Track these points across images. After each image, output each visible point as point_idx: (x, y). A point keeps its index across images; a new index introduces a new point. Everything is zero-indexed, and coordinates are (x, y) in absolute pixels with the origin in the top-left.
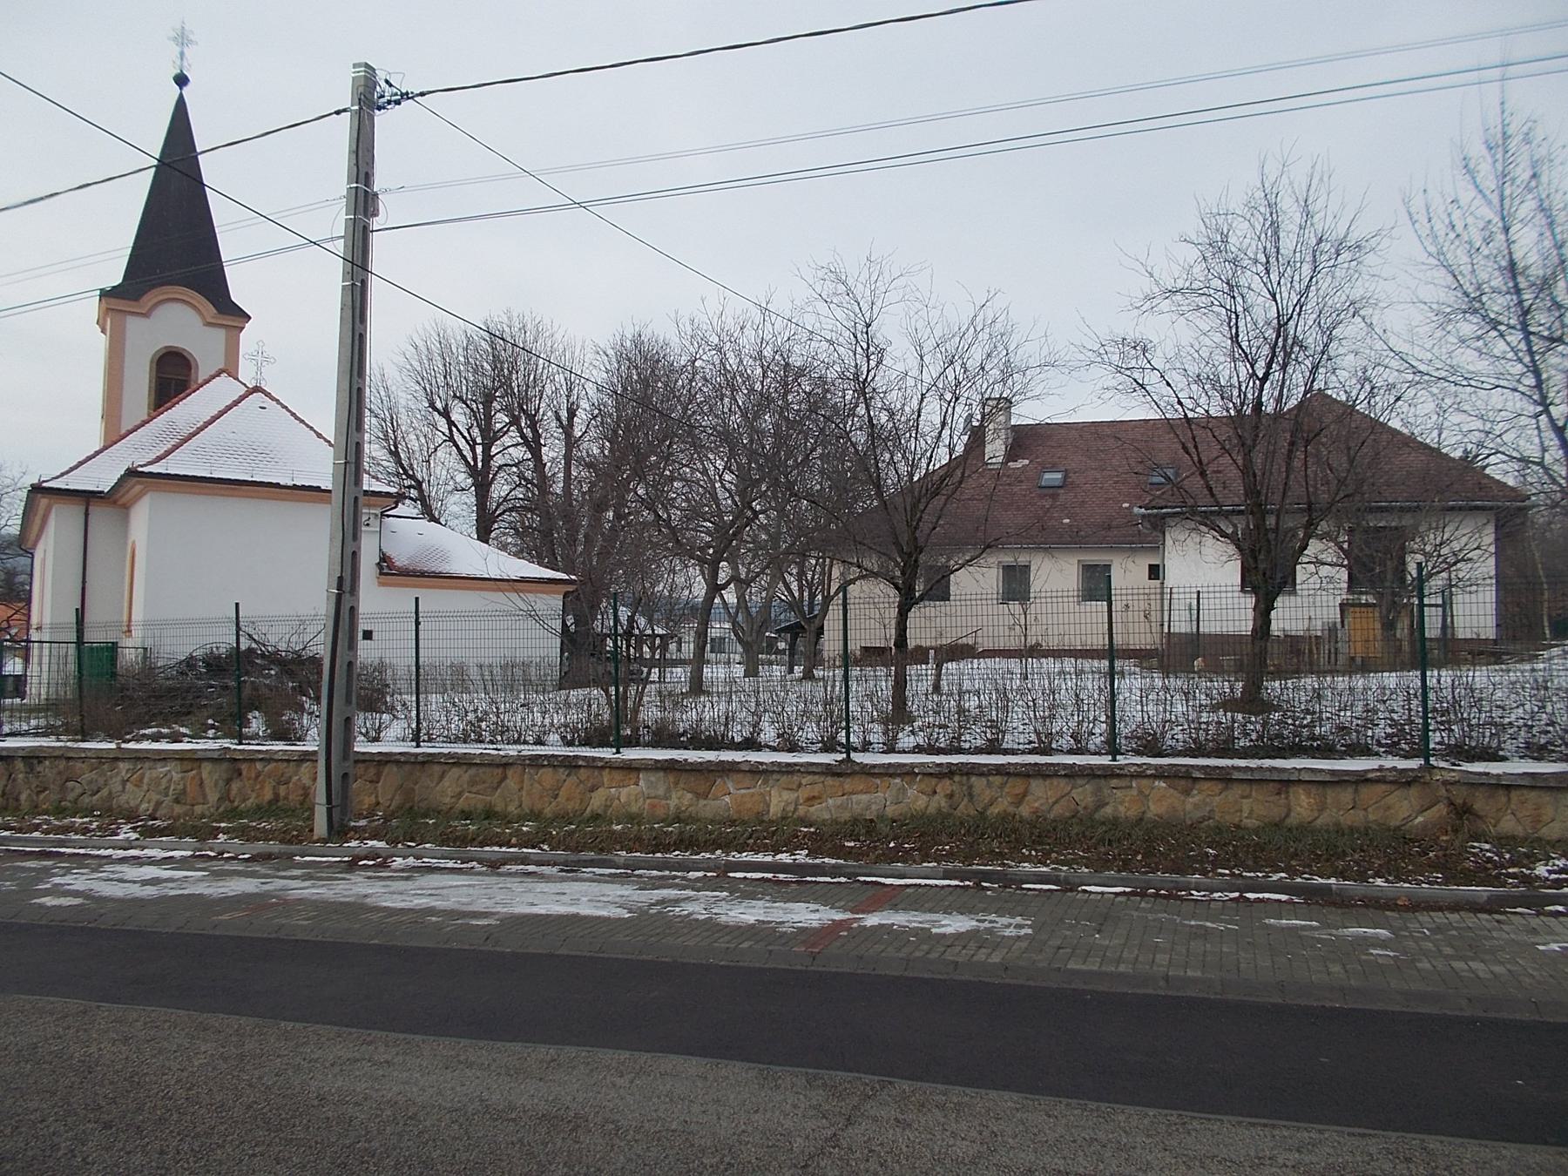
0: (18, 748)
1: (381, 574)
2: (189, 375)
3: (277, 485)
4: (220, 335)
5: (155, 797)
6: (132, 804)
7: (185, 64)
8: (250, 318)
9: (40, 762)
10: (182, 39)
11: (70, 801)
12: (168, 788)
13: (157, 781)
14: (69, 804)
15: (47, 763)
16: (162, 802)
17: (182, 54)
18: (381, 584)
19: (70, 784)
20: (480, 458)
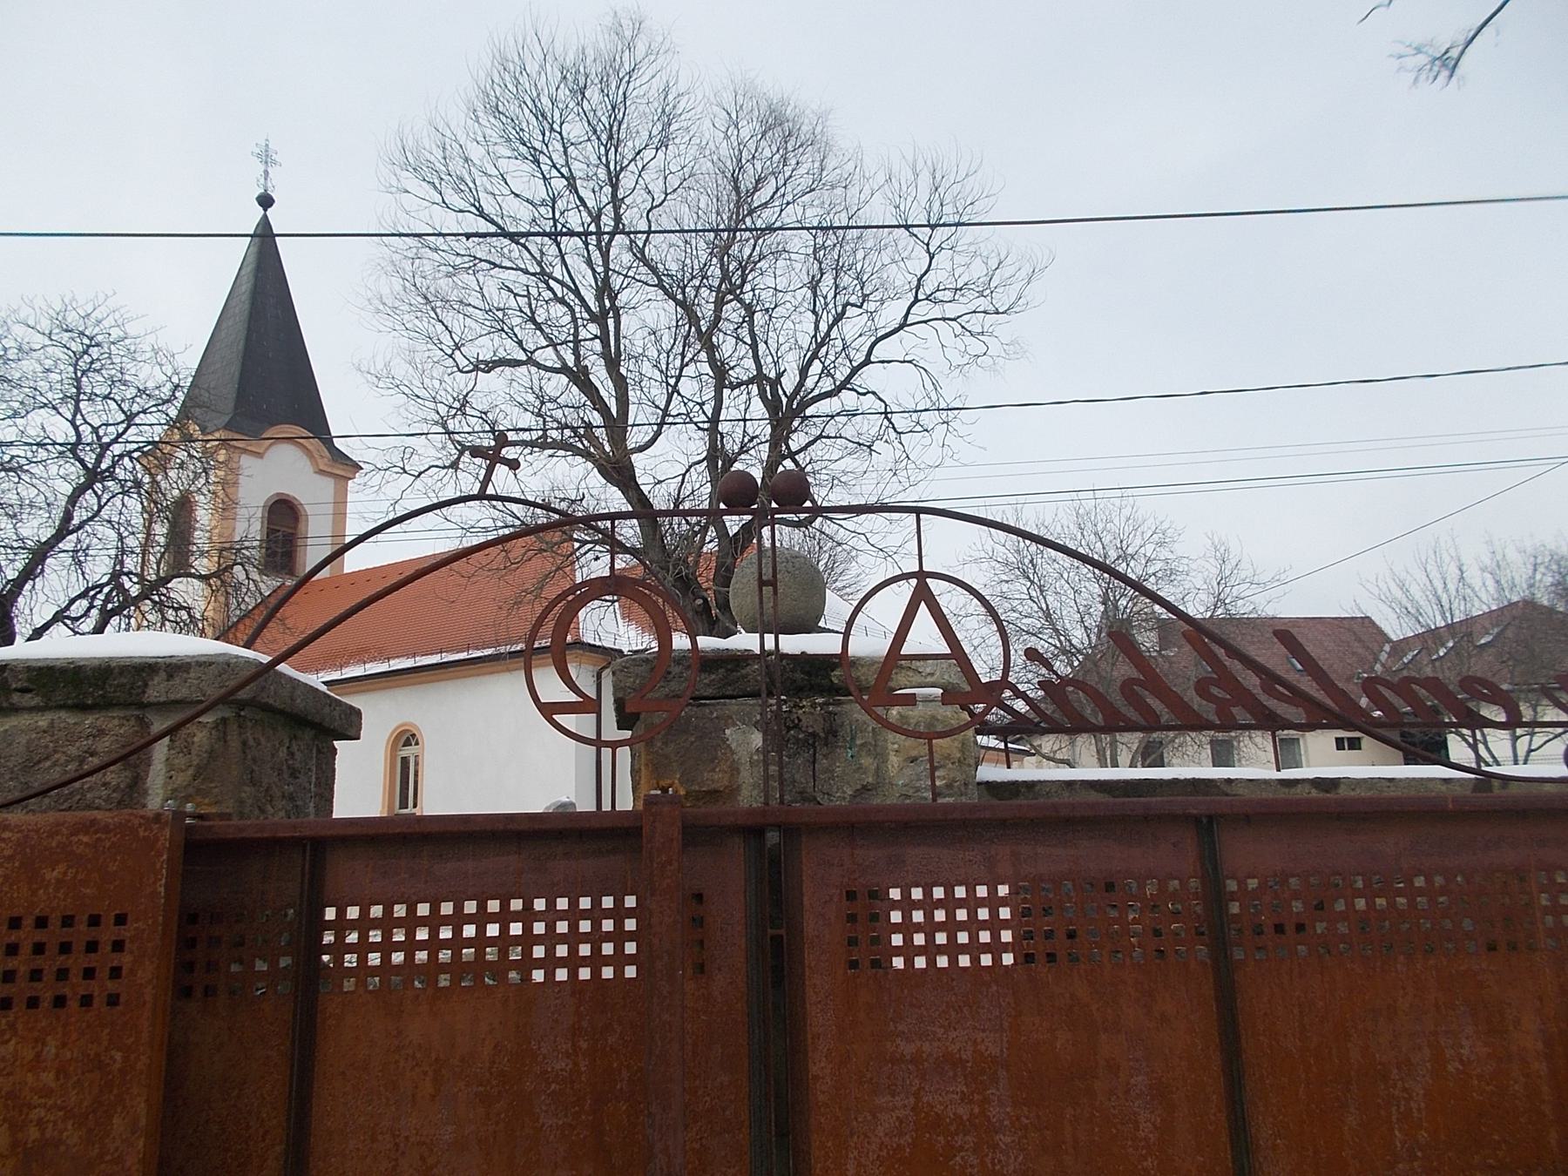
2: (295, 528)
7: (269, 185)
10: (266, 157)
17: (266, 173)
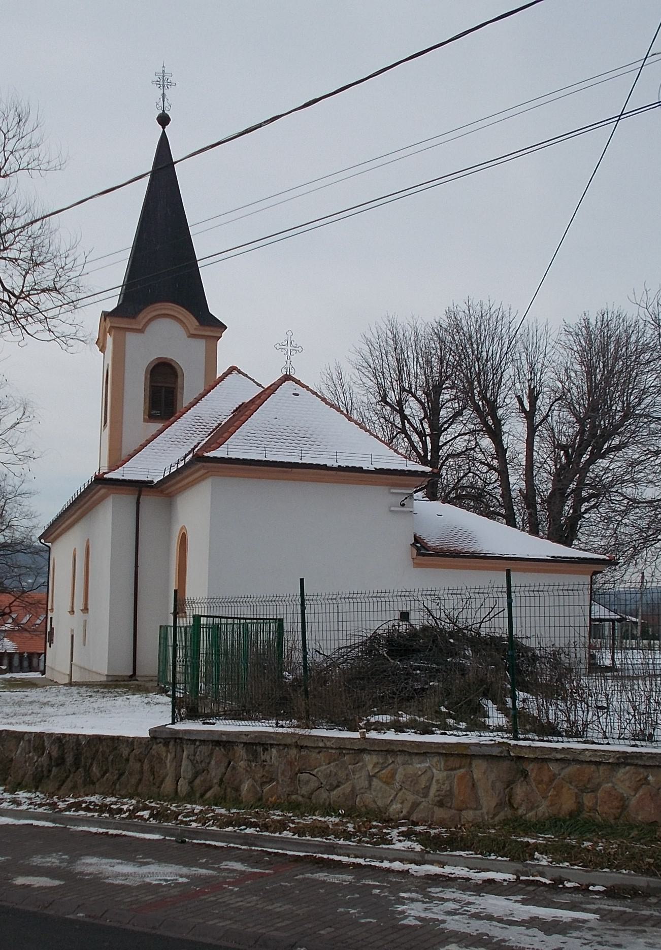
0: (241, 733)
1: (419, 554)
2: (176, 382)
3: (324, 467)
4: (200, 346)
5: (411, 798)
6: (380, 803)
7: (166, 104)
8: (226, 328)
9: (265, 750)
11: (303, 796)
12: (428, 788)
13: (414, 779)
14: (300, 799)
15: (274, 751)
16: (419, 804)
17: (164, 95)
18: (417, 565)
19: (304, 777)
20: (429, 447)
